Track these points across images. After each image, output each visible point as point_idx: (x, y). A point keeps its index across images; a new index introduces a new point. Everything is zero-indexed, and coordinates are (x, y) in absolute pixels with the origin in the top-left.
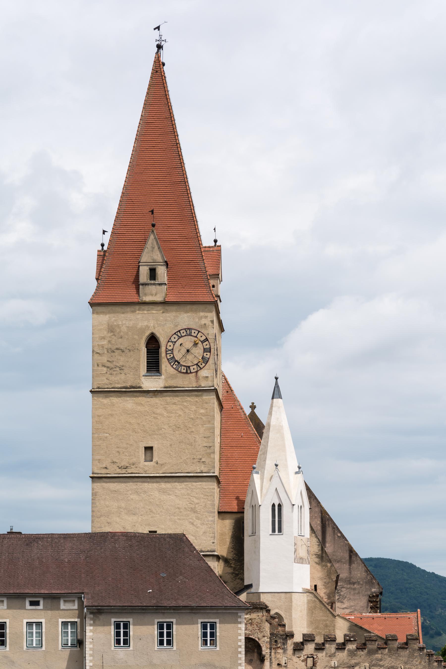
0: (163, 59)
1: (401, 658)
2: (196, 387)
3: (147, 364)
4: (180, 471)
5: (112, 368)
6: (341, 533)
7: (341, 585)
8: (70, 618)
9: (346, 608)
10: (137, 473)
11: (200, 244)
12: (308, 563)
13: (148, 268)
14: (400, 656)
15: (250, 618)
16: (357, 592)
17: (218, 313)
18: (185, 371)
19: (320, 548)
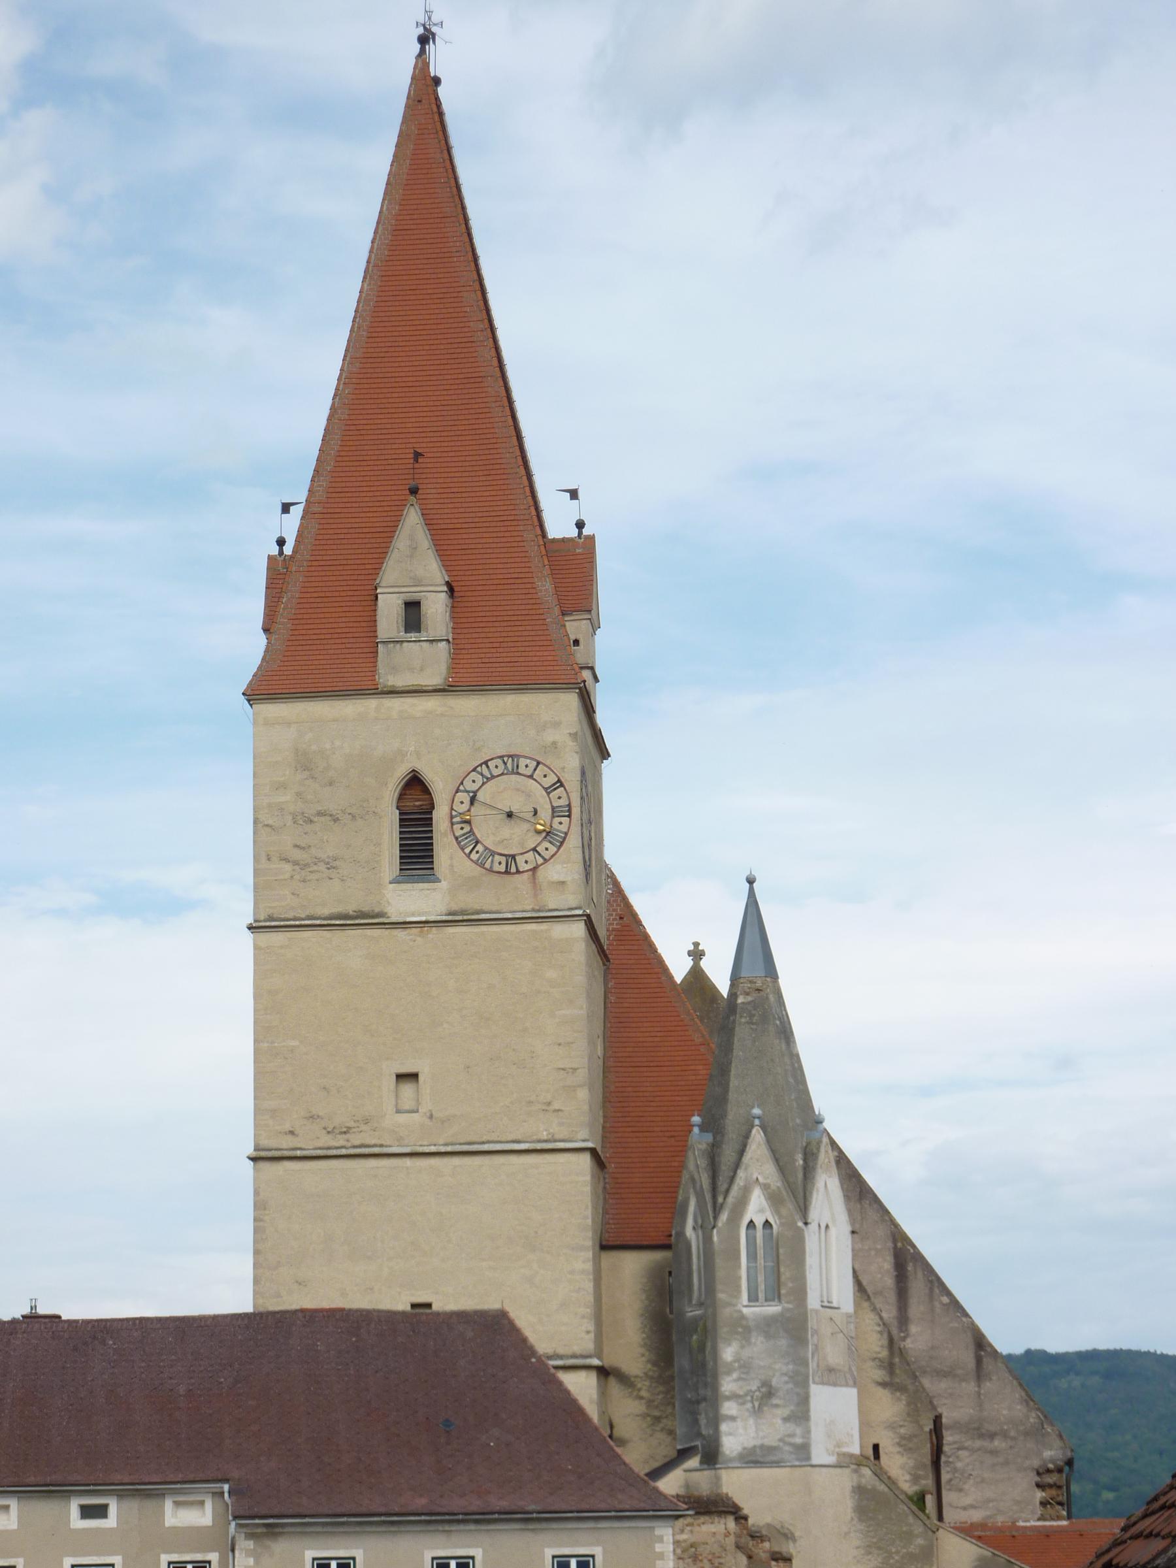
0: (437, 68)
2: (533, 910)
3: (401, 851)
4: (494, 1137)
5: (307, 865)
6: (949, 1293)
7: (955, 1443)
8: (192, 1551)
9: (973, 1507)
10: (375, 1146)
11: (544, 534)
12: (851, 1382)
13: (400, 602)
15: (693, 1539)
16: (1001, 1460)
17: (588, 709)
18: (502, 868)
19: (885, 1342)
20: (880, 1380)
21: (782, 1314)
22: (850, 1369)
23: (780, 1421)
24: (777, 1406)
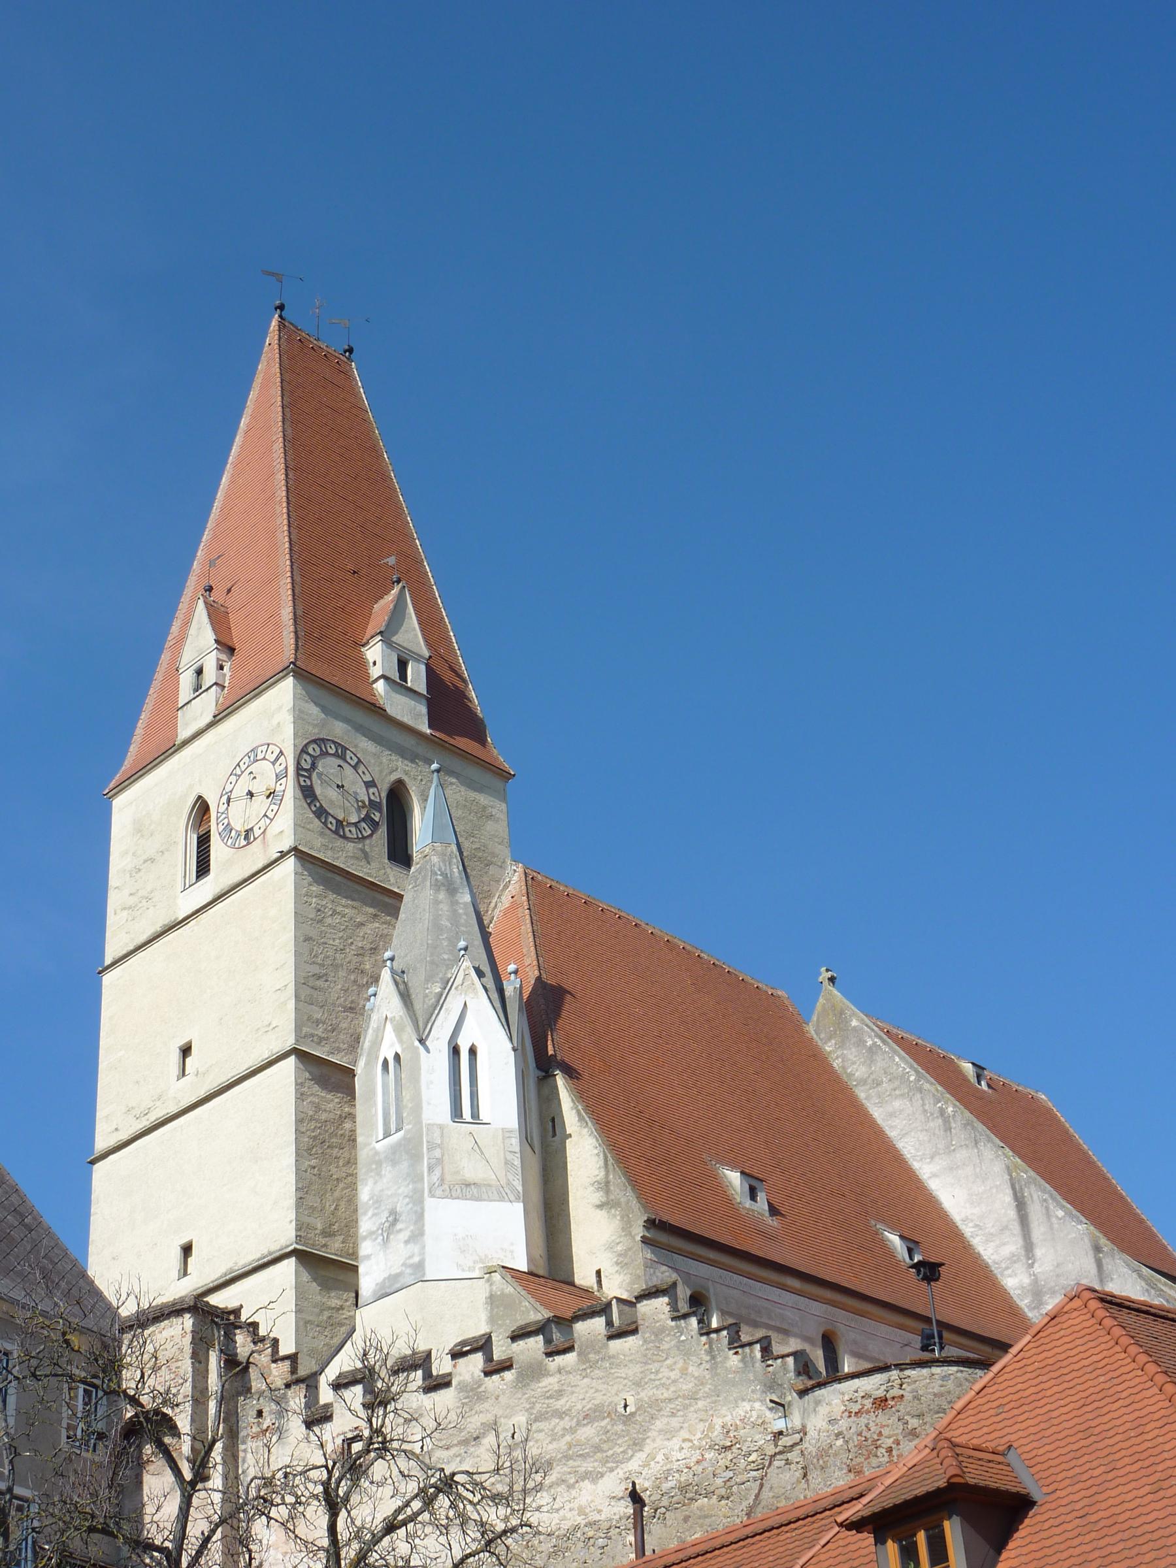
1: (622, 1372)
14: (618, 1365)
19: (602, 1163)
20: (599, 1203)
21: (404, 1138)
22: (509, 1183)
23: (402, 1245)
24: (401, 1230)
